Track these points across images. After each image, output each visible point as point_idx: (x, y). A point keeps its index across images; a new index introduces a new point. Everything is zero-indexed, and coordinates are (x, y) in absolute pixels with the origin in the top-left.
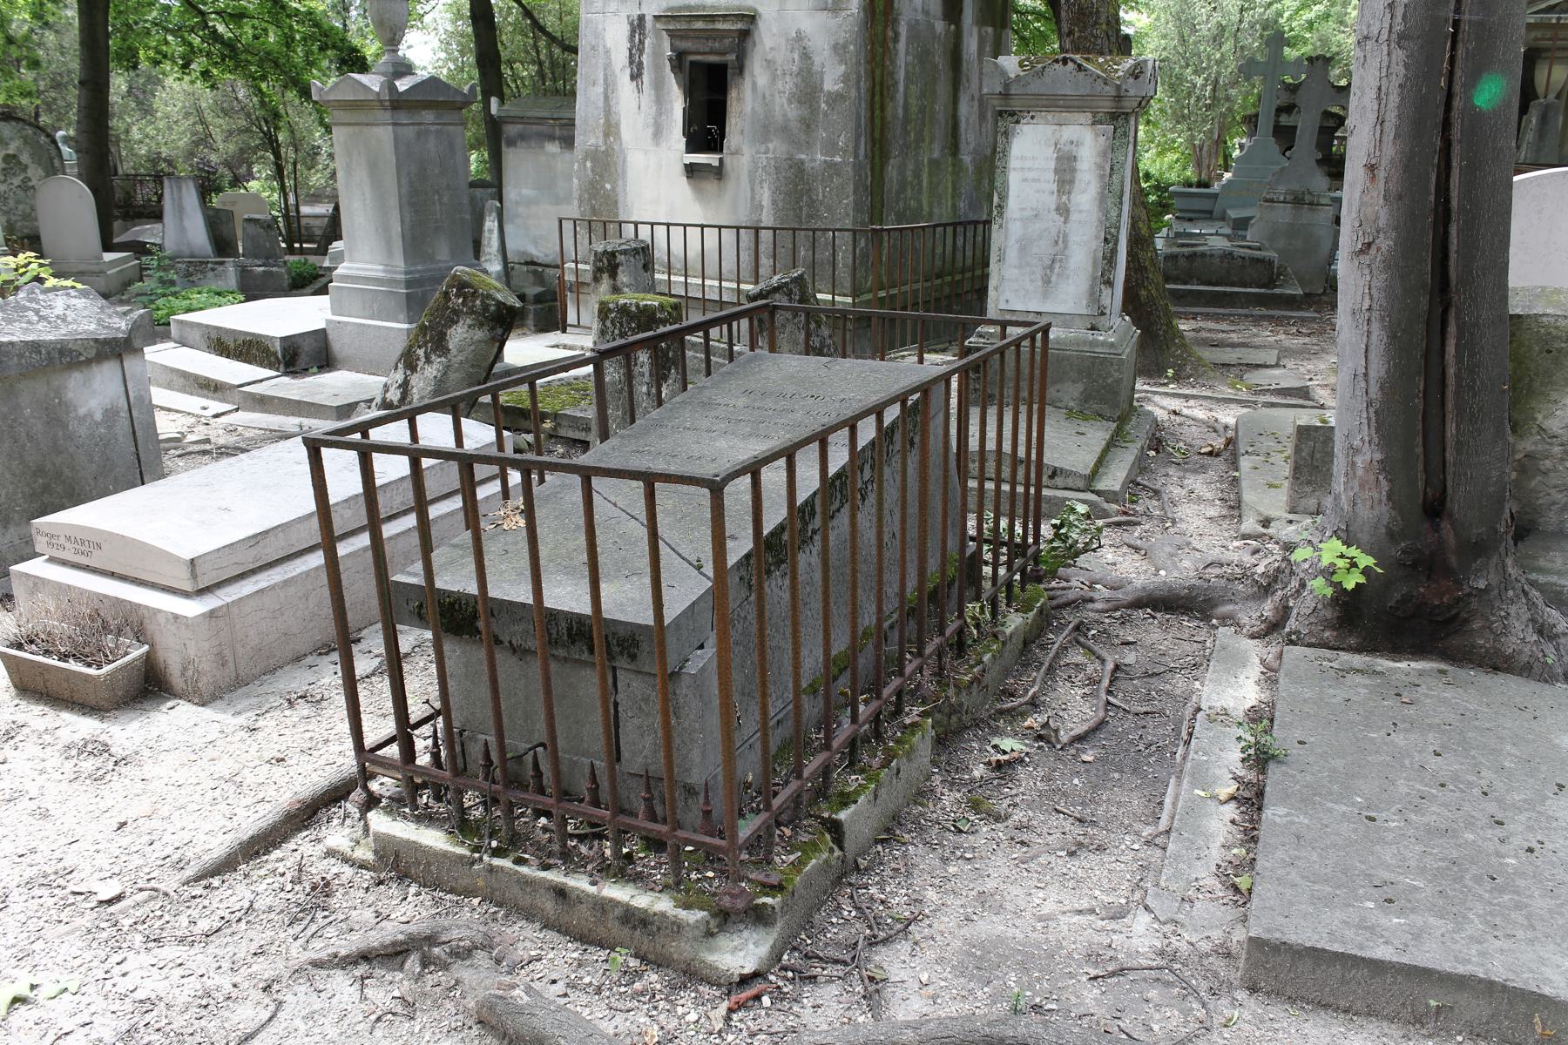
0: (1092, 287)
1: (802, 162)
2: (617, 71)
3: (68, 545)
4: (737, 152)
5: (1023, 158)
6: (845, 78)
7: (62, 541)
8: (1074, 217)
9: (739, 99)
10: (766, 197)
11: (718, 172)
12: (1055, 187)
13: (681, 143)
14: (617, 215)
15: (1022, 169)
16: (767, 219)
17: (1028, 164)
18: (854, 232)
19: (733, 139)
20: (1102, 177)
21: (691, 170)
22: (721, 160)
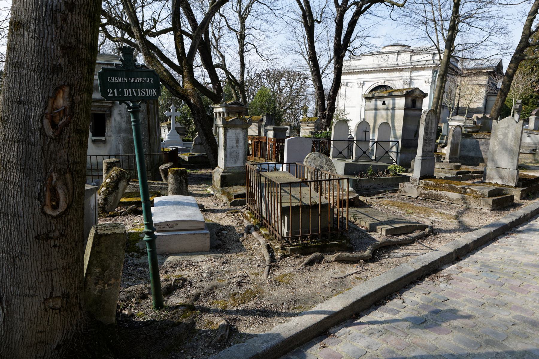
4: (110, 136)
7: (164, 226)
9: (110, 123)
10: (121, 147)
19: (108, 132)
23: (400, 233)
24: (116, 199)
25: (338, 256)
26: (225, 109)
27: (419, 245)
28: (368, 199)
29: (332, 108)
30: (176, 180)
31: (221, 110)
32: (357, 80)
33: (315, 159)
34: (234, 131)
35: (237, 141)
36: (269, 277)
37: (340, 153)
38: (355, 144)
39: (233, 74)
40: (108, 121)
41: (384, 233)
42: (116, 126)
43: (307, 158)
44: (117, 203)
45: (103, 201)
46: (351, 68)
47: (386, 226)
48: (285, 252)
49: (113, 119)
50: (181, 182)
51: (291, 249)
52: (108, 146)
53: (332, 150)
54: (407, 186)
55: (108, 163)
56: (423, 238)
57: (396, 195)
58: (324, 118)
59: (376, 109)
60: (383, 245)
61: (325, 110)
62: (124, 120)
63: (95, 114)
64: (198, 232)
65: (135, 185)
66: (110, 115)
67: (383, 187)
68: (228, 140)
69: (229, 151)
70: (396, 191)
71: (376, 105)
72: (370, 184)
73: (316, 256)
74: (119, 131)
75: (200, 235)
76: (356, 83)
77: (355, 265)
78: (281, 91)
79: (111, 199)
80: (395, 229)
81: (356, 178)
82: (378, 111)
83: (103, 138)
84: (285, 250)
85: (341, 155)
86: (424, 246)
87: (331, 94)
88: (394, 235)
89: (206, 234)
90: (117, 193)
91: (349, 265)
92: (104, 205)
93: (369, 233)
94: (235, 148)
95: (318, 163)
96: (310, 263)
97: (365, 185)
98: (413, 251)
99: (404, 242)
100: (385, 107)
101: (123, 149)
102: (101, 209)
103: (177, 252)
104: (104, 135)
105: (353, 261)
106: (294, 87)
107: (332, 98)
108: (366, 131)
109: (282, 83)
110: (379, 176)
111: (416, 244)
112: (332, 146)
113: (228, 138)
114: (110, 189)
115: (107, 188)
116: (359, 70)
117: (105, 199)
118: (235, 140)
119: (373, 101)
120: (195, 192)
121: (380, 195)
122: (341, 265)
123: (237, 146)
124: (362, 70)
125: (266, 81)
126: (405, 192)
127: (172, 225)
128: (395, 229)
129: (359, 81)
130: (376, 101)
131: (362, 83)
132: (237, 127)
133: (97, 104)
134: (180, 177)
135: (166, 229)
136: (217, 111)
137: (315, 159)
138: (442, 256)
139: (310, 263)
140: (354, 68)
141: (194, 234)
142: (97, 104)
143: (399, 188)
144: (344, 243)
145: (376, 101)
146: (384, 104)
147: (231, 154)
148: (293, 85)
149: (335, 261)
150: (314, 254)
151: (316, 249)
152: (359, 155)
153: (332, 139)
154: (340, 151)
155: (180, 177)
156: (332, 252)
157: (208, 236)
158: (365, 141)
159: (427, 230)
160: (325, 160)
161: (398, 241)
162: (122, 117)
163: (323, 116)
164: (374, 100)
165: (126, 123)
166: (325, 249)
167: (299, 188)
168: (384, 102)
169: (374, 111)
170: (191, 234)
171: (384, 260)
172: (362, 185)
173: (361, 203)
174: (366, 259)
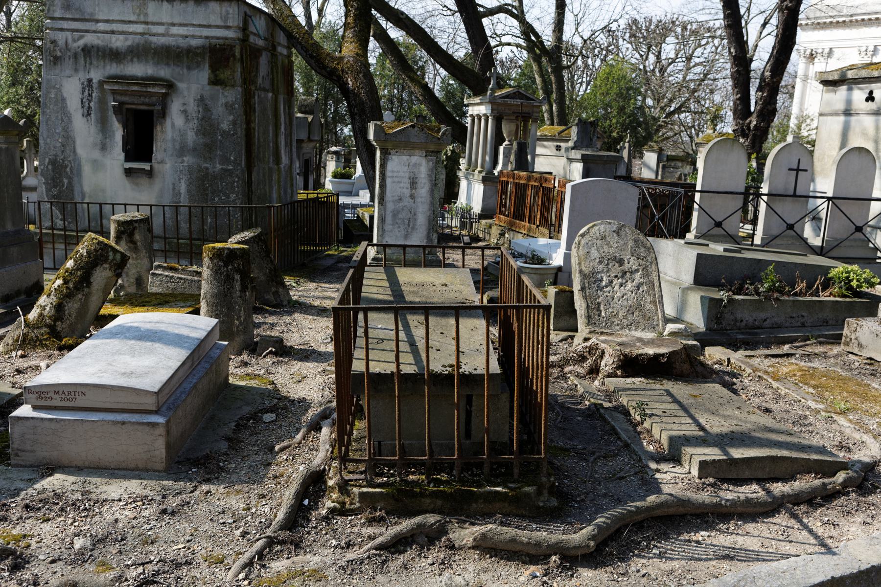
0: (428, 233)
1: (207, 169)
2: (72, 111)
3: (57, 396)
4: (162, 162)
5: (393, 172)
6: (234, 123)
7: (51, 394)
8: (419, 200)
9: (162, 132)
10: (183, 188)
11: (150, 174)
12: (409, 186)
13: (122, 156)
14: (73, 198)
15: (392, 177)
16: (184, 200)
17: (395, 174)
18: (52, 203)
19: (157, 155)
20: (431, 181)
21: (129, 172)
22: (151, 166)
23: (747, 475)
24: (84, 306)
25: (484, 536)
26: (489, 107)
27: (792, 522)
28: (737, 357)
29: (768, 111)
30: (216, 272)
31: (483, 110)
32: (859, 43)
33: (603, 238)
34: (405, 158)
35: (413, 183)
36: (241, 576)
37: (719, 224)
38: (763, 207)
39: (537, 26)
40: (159, 128)
41: (695, 472)
42: (174, 140)
43: (583, 235)
44: (90, 315)
45: (53, 312)
46: (845, 12)
47: (707, 450)
48: (347, 500)
49: (168, 122)
50: (229, 279)
51: (362, 495)
52: (158, 184)
53: (695, 215)
54: (865, 328)
55: (120, 223)
56: (818, 500)
57: (836, 350)
58: (744, 135)
59: (848, 112)
60: (658, 513)
61: (750, 114)
62: (191, 125)
63: (136, 111)
64: (136, 418)
65: (172, 277)
66: (163, 114)
67: (803, 325)
68: (388, 181)
69: (390, 206)
70: (837, 339)
71: (849, 102)
72: (763, 315)
73: (420, 526)
74: (182, 151)
75: (140, 428)
76: (856, 49)
77: (532, 568)
78: (662, 70)
79: (72, 307)
80: (733, 462)
81: (722, 295)
82: (853, 119)
83: (146, 166)
84: (348, 494)
85: (718, 231)
86: (806, 527)
87: (768, 74)
88: (724, 480)
89: (154, 425)
90: (87, 296)
91: (513, 565)
92: (55, 321)
93: (653, 466)
94: (407, 202)
95: (611, 251)
96: (397, 545)
97: (747, 316)
98: (752, 544)
99: (740, 509)
100: (871, 106)
101: (189, 191)
102: (47, 330)
103: (80, 464)
104: (148, 158)
105: (528, 555)
106: (697, 60)
107: (768, 84)
108: (798, 170)
109: (669, 49)
110: (795, 294)
111: (782, 519)
112: (696, 206)
113: (388, 174)
114: (71, 285)
115: (66, 282)
116: (866, 17)
117: (59, 308)
118: (407, 180)
119: (843, 90)
120: (317, 303)
121: (786, 348)
122: (487, 562)
123: (412, 197)
124: (873, 17)
125: (629, 46)
126: (860, 345)
127: (69, 393)
128: (733, 462)
129: (864, 44)
130: (850, 89)
131: (871, 48)
132: (413, 148)
133: (136, 88)
134: (226, 265)
135: (56, 402)
136: (475, 113)
137: (603, 238)
138: (838, 574)
139: (397, 545)
140: (852, 12)
141: (123, 423)
142: (136, 88)
143: (846, 332)
144: (528, 495)
145: (850, 89)
146: (870, 98)
147: (395, 214)
148: (691, 56)
149: (474, 548)
150: (418, 519)
151: (439, 502)
152: (775, 232)
153: (698, 188)
154: (718, 219)
155: (226, 265)
156: (472, 518)
157: (161, 430)
158: (794, 195)
159: (841, 477)
160: (631, 243)
161: (718, 505)
162: (187, 120)
163: (743, 130)
164: (845, 87)
165: (197, 134)
166: (463, 507)
167: (452, 321)
168: (871, 93)
169: (842, 118)
170: (115, 423)
171: (637, 563)
172: (739, 316)
173: (699, 369)
174: (573, 553)
